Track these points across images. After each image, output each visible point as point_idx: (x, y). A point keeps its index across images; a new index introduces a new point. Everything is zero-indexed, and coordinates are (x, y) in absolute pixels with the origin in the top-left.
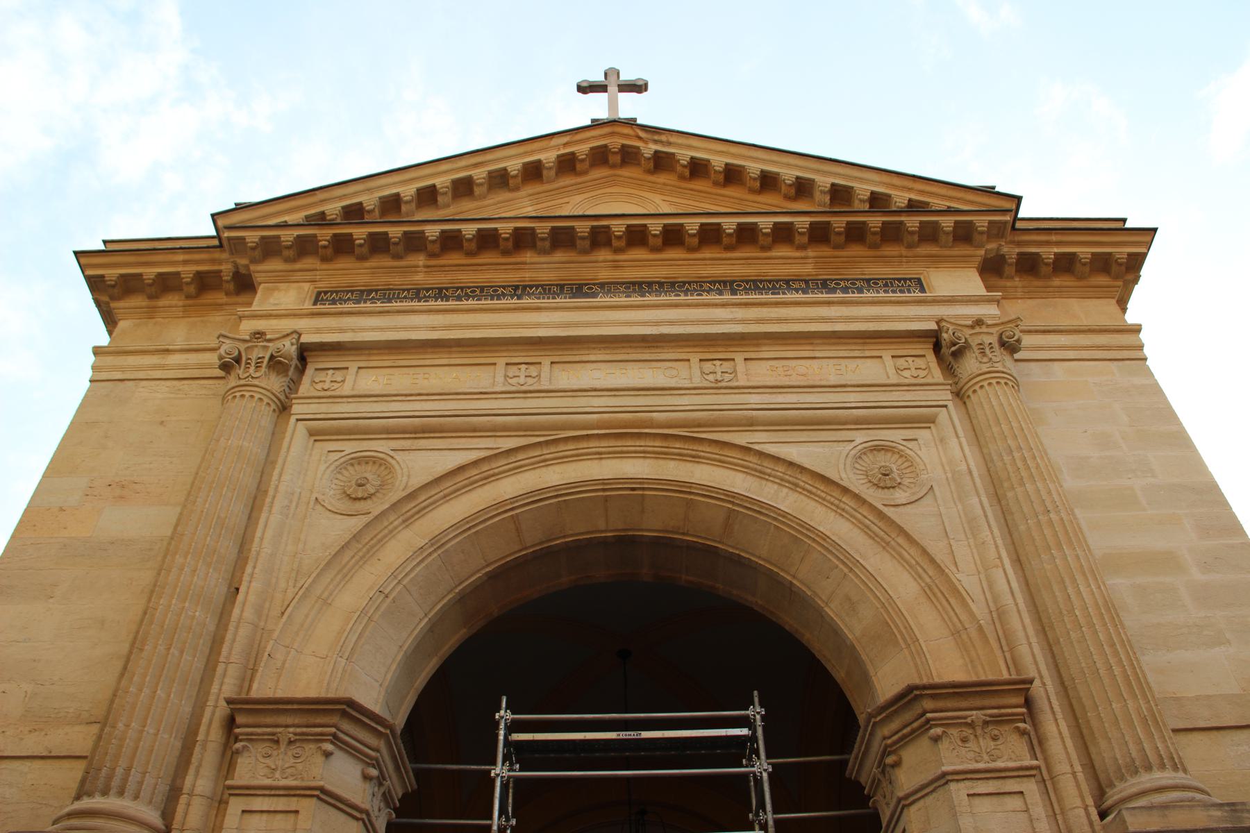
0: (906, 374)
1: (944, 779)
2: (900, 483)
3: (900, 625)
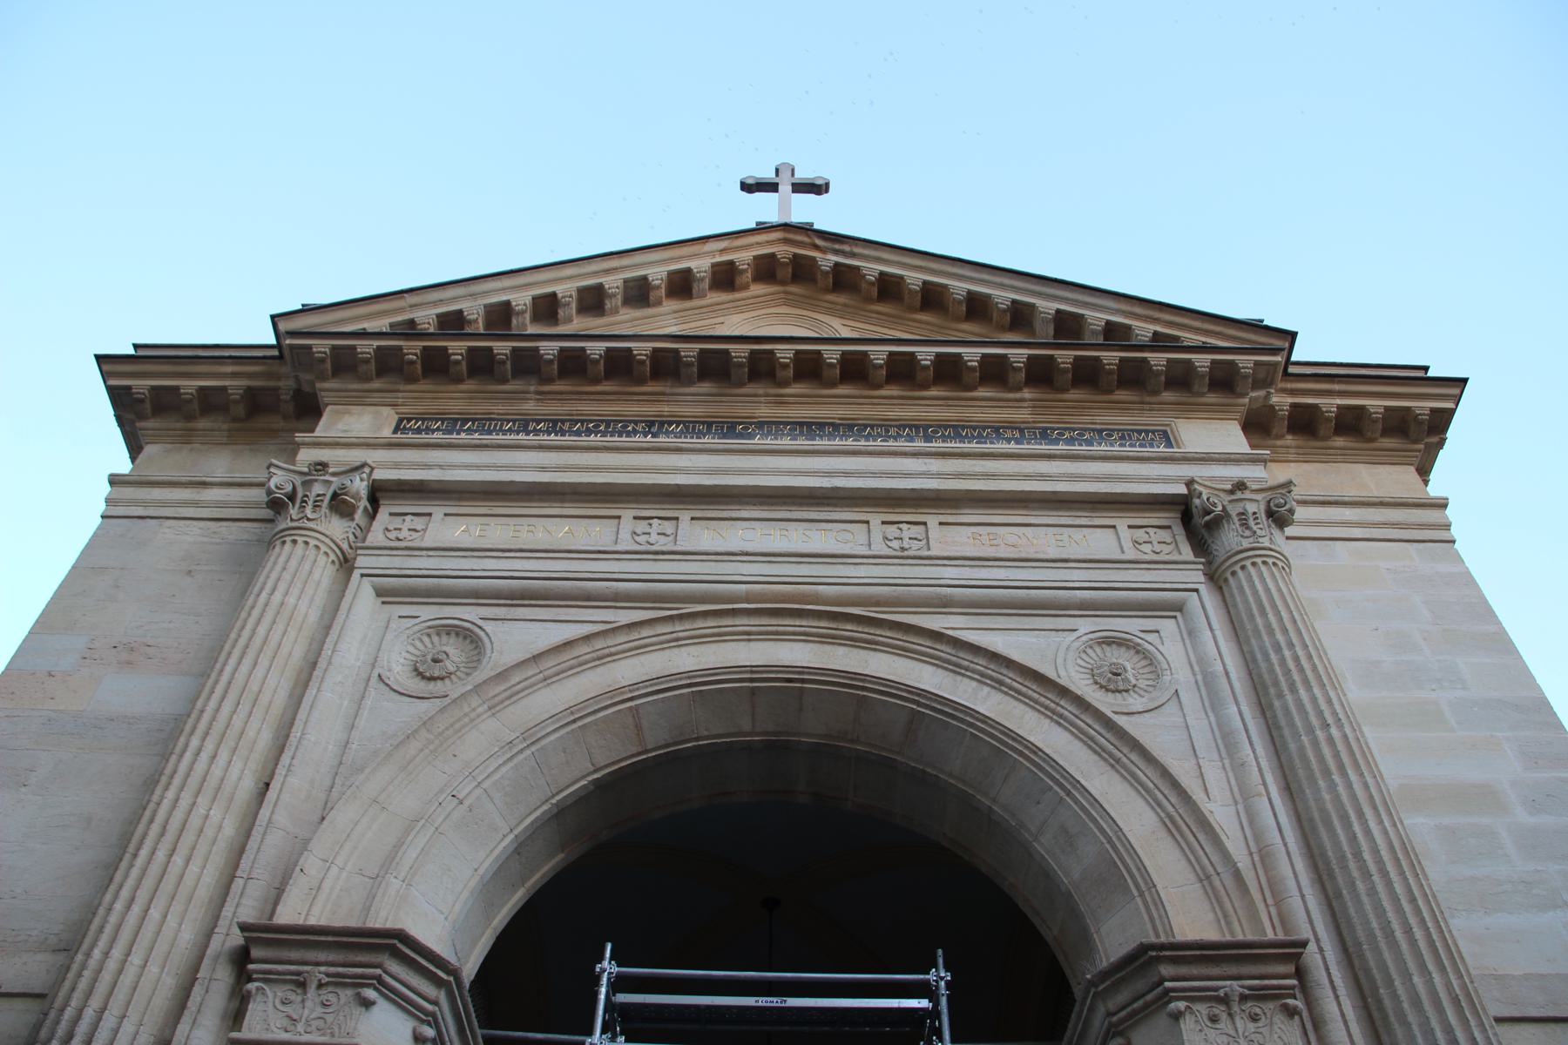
0: (1146, 548)
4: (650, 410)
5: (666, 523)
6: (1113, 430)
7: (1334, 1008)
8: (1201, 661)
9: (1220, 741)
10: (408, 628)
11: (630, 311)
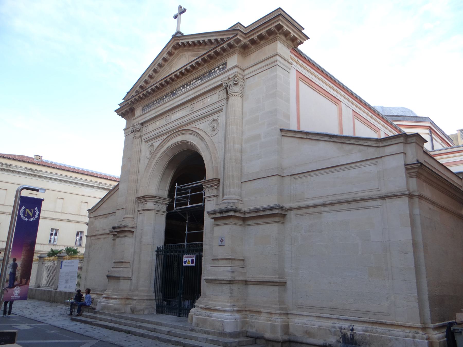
2: (216, 129)
4: (164, 94)
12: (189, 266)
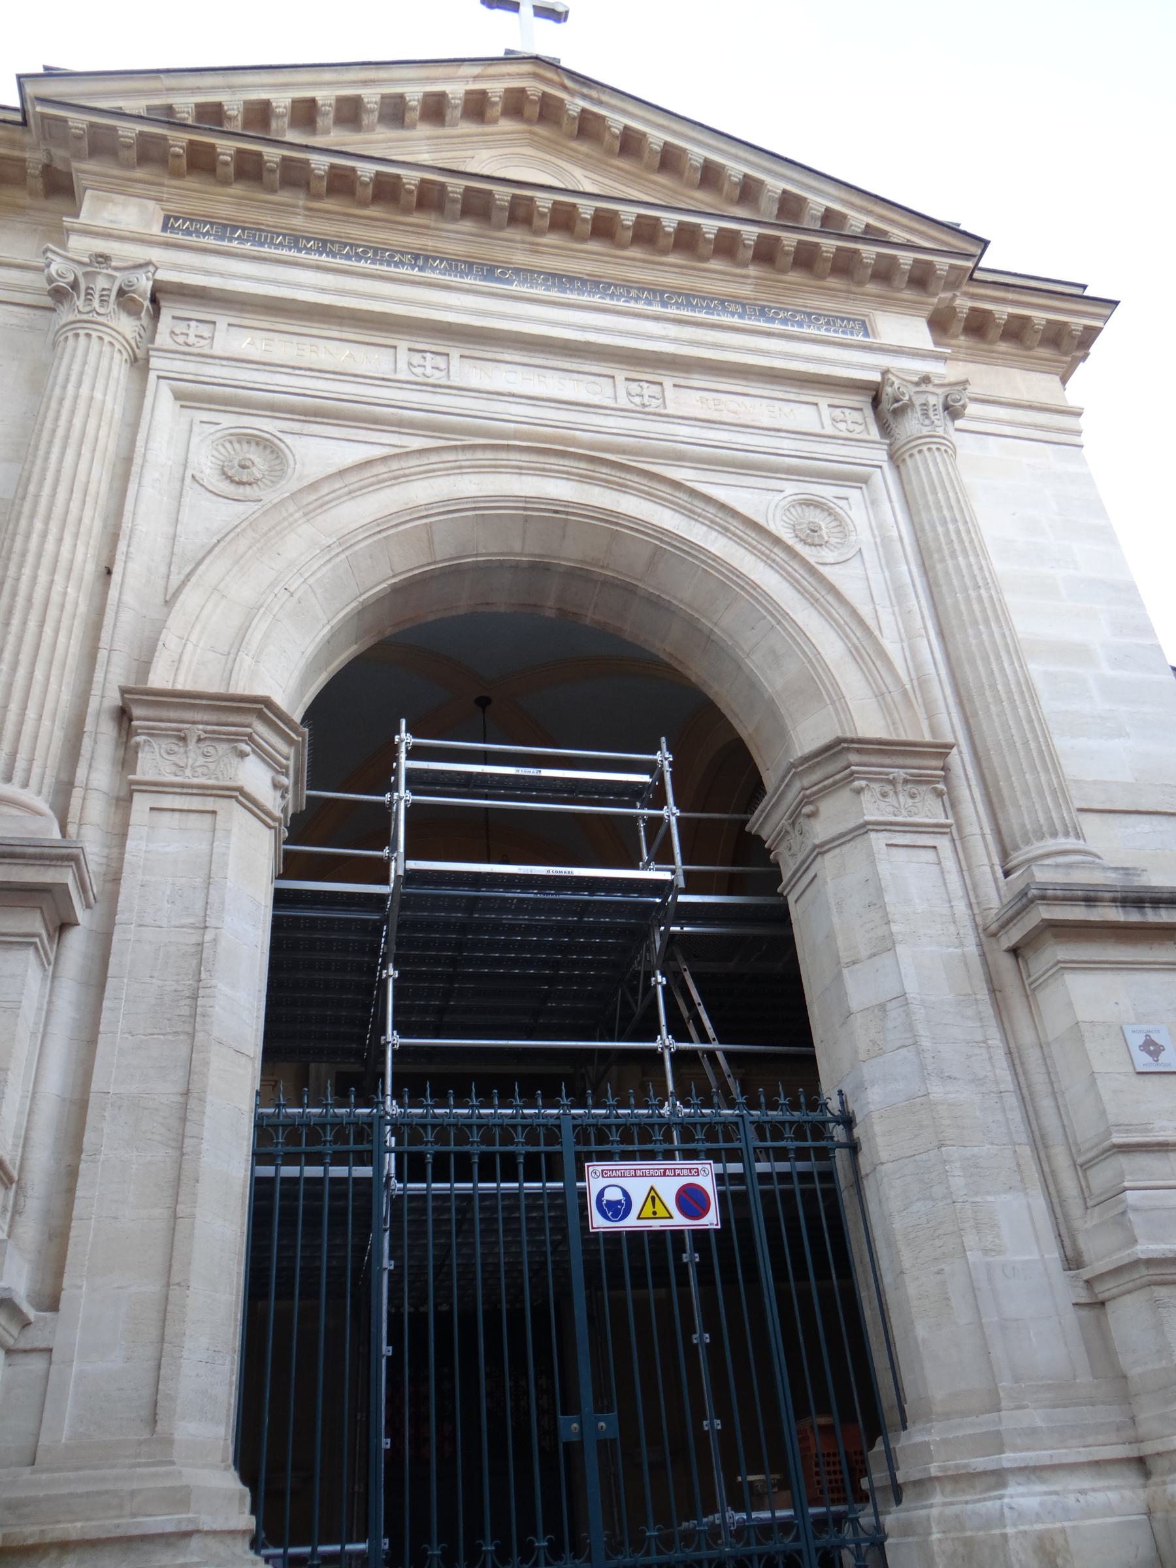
0: (842, 426)
1: (864, 829)
3: (827, 682)
5: (438, 358)
6: (821, 315)
7: (967, 793)
8: (881, 526)
9: (892, 593)
10: (211, 434)
11: (385, 130)
12: (657, 1236)
